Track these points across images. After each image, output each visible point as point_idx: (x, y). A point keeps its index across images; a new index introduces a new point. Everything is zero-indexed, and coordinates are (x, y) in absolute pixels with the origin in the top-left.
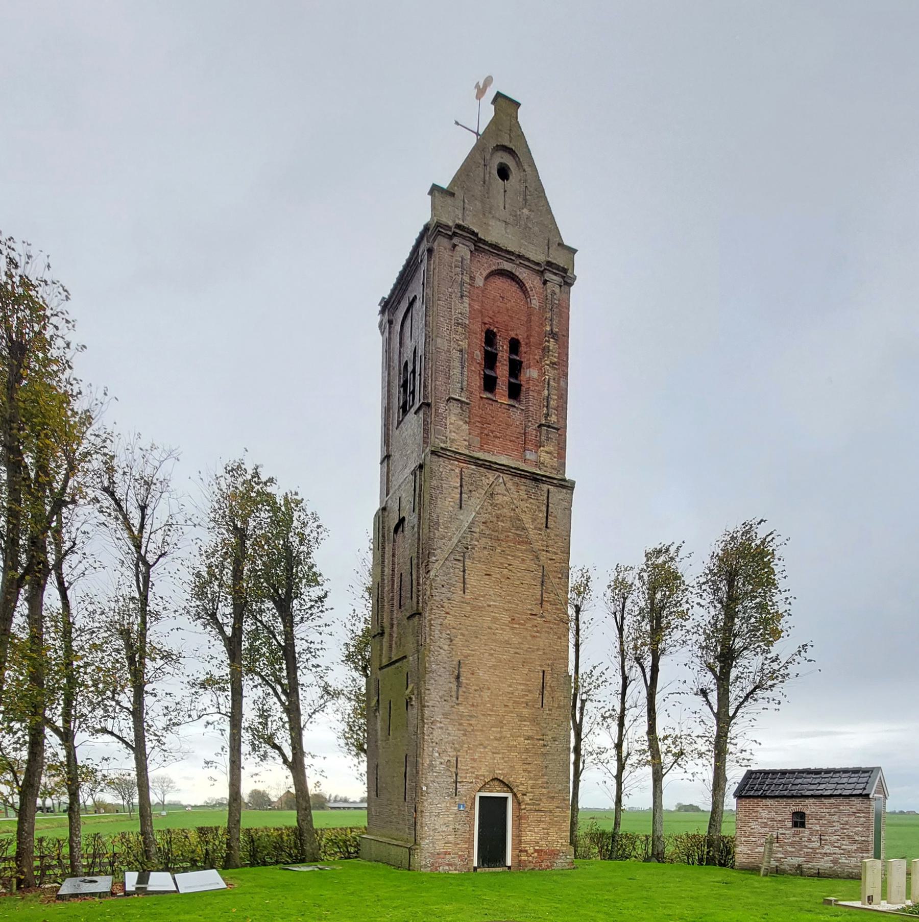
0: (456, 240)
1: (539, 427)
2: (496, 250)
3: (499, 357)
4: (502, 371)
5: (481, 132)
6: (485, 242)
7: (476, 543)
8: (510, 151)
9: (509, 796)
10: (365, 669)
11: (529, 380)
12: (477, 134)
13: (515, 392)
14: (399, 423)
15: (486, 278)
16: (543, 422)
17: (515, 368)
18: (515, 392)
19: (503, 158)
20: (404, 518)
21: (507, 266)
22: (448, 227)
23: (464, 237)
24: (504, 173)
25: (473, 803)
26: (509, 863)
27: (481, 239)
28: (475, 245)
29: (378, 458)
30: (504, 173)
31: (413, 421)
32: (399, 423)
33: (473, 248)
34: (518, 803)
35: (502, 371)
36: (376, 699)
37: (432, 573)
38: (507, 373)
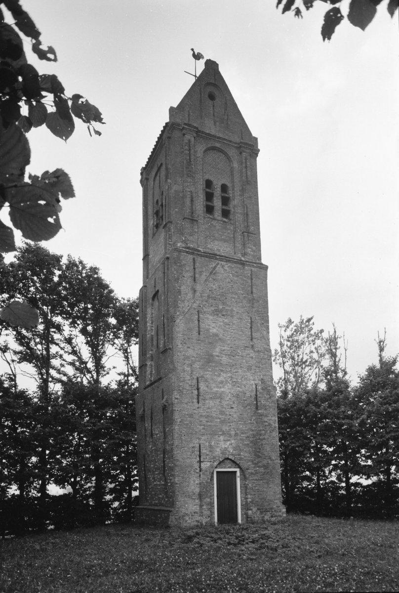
0: (184, 131)
1: (242, 233)
2: (209, 137)
3: (215, 194)
4: (217, 203)
5: (198, 75)
6: (203, 132)
7: (206, 303)
8: (215, 85)
9: (238, 470)
10: (287, 457)
11: (235, 206)
12: (195, 76)
13: (226, 213)
14: (154, 235)
15: (205, 151)
16: (245, 231)
17: (225, 201)
18: (226, 213)
19: (210, 89)
20: (158, 291)
21: (218, 145)
22: (179, 125)
23: (190, 130)
24: (212, 97)
25: (212, 477)
26: (240, 521)
27: (200, 131)
28: (197, 134)
29: (141, 256)
30: (212, 97)
31: (162, 234)
32: (154, 235)
33: (195, 135)
34: (244, 477)
35: (217, 203)
36: (143, 409)
37: (272, 526)
38: (220, 203)
